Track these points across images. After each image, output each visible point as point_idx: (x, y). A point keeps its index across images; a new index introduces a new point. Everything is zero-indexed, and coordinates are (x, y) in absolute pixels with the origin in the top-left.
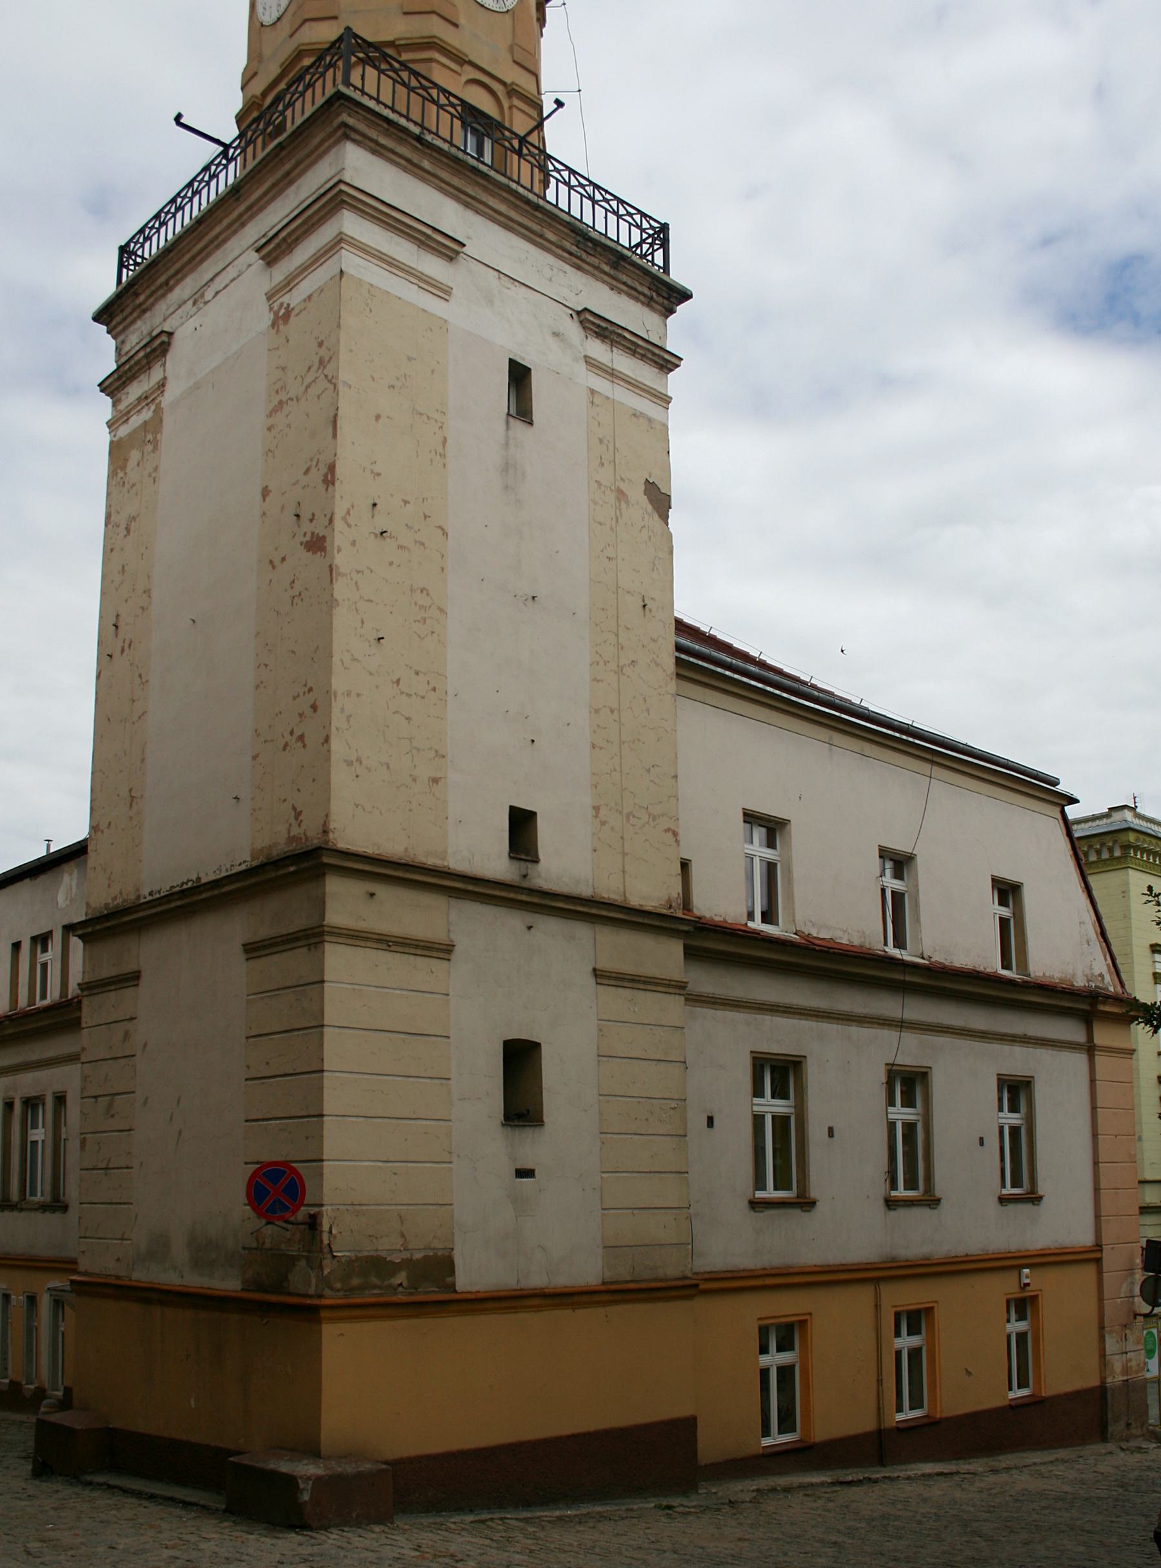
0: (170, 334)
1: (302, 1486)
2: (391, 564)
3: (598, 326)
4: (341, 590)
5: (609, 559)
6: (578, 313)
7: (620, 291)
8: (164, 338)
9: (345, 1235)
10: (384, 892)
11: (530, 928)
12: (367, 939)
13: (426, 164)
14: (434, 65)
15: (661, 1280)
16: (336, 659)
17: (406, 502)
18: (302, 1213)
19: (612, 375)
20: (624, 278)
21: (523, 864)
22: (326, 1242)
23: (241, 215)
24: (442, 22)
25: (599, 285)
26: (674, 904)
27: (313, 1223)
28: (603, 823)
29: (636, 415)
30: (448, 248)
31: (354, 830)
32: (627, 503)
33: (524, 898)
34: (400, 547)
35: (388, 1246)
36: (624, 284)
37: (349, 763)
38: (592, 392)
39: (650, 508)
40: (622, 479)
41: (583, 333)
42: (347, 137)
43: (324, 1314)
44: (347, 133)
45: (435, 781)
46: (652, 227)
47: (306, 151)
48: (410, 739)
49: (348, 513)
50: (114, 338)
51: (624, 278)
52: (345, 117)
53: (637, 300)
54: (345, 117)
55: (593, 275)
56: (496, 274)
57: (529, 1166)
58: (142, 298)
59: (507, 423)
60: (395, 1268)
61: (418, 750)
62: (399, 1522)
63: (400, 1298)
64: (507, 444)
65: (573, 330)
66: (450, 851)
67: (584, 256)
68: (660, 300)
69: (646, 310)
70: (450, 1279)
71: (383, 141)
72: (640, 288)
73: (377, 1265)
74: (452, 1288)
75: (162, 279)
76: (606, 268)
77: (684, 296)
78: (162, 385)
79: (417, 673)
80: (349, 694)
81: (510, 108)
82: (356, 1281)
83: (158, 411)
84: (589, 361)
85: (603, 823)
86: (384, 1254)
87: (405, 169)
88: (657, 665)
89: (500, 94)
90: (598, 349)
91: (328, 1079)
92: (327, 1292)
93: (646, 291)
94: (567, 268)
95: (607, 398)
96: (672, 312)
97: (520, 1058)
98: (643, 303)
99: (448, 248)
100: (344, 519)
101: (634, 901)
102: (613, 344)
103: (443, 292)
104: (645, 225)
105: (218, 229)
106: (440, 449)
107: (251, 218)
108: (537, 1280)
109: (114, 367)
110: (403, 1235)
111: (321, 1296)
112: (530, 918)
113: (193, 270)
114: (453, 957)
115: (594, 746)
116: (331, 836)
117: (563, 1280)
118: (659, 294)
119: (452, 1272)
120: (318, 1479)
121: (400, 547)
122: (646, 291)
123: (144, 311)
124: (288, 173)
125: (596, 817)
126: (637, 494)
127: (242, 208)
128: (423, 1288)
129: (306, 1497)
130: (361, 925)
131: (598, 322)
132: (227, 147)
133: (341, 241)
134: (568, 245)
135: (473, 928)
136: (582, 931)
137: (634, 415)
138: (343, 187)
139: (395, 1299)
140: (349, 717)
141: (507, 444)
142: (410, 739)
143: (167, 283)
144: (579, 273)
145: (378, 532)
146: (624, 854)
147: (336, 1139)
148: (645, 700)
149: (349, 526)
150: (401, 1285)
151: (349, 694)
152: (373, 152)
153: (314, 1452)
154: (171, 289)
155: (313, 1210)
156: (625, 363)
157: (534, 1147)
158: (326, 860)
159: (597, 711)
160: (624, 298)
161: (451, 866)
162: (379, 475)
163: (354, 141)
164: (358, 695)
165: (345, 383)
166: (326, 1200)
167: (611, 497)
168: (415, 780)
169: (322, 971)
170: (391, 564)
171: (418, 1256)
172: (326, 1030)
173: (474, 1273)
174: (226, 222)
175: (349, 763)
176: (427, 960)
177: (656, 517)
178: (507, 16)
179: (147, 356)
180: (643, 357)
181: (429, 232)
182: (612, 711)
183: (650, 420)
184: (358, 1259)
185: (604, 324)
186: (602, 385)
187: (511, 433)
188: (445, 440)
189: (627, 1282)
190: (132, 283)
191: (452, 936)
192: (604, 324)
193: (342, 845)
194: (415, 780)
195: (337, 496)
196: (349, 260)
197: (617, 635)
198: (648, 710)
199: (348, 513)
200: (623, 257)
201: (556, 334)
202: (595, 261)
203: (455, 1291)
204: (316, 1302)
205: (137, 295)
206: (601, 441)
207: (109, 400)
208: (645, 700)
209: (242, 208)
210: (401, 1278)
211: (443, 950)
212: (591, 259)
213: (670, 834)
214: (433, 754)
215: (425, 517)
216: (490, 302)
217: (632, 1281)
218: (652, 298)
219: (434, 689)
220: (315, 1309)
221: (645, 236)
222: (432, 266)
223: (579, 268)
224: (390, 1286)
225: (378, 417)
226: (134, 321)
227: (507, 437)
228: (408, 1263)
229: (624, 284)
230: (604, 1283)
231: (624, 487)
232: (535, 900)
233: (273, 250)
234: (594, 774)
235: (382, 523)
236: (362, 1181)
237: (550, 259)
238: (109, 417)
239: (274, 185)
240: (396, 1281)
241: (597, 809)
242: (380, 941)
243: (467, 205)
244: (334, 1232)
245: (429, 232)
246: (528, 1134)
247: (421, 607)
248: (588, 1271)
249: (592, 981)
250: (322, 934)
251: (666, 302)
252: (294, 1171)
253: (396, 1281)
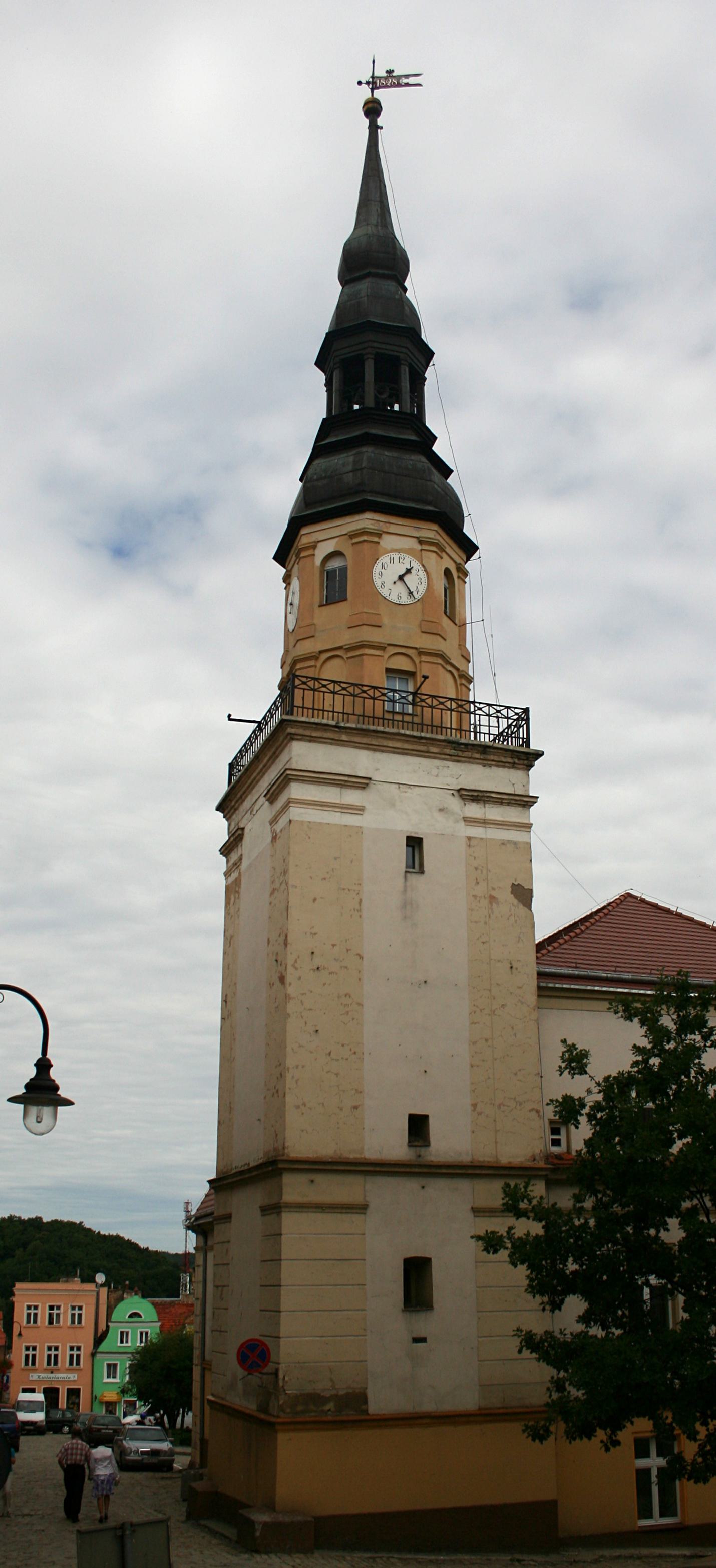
0: (243, 829)
1: (257, 1527)
2: (325, 984)
3: (472, 796)
4: (291, 1008)
5: (484, 943)
6: (459, 790)
7: (490, 766)
8: (240, 832)
9: (293, 1382)
10: (319, 1178)
11: (423, 1187)
12: (308, 1207)
13: (344, 738)
14: (364, 657)
15: (527, 1407)
16: (289, 1049)
17: (334, 945)
18: (270, 1368)
19: (484, 823)
20: (492, 757)
21: (418, 1149)
22: (281, 1384)
23: (262, 770)
24: (370, 628)
25: (475, 767)
26: (537, 1158)
27: (276, 1373)
28: (480, 1114)
29: (503, 843)
30: (362, 783)
31: (302, 1141)
32: (498, 903)
33: (416, 1170)
34: (331, 973)
35: (322, 1386)
36: (493, 761)
37: (298, 1107)
38: (469, 838)
39: (515, 901)
40: (494, 889)
41: (462, 802)
42: (293, 739)
43: (278, 1427)
44: (292, 737)
45: (356, 1107)
46: (516, 714)
47: (279, 744)
48: (338, 1086)
49: (296, 961)
50: (227, 820)
51: (492, 757)
52: (290, 730)
53: (504, 767)
54: (290, 730)
55: (469, 762)
56: (397, 786)
57: (422, 1335)
58: (233, 803)
59: (405, 877)
60: (326, 1400)
61: (344, 1091)
62: (317, 1554)
63: (330, 1418)
64: (405, 891)
65: (455, 804)
66: (366, 1147)
67: (460, 754)
68: (521, 762)
69: (512, 771)
70: (363, 1407)
71: (314, 735)
72: (504, 760)
73: (315, 1399)
74: (366, 1412)
75: (239, 795)
76: (477, 756)
77: (539, 755)
78: (241, 859)
79: (343, 1045)
80: (297, 1067)
81: (420, 662)
82: (300, 1408)
83: (240, 873)
84: (468, 820)
85: (480, 1114)
86: (318, 1392)
87: (331, 744)
88: (522, 1003)
89: (413, 656)
90: (474, 810)
91: (283, 1291)
92: (282, 1414)
93: (510, 760)
94: (450, 764)
95: (482, 839)
96: (532, 766)
97: (416, 1272)
98: (509, 768)
99: (362, 783)
100: (293, 966)
101: (504, 1160)
102: (485, 802)
103: (359, 810)
104: (511, 714)
105: (255, 775)
106: (357, 907)
107: (266, 771)
108: (428, 1407)
109: (227, 838)
110: (332, 1380)
111: (278, 1417)
112: (423, 1181)
113: (250, 792)
114: (368, 1212)
115: (472, 1066)
116: (286, 1151)
117: (447, 1407)
118: (519, 759)
119: (365, 1401)
120: (265, 1524)
121: (331, 973)
122: (510, 760)
123: (236, 810)
124: (275, 753)
125: (474, 1110)
126: (505, 896)
127: (261, 766)
128: (345, 1411)
129: (258, 1534)
130: (305, 1200)
131: (470, 793)
132: (259, 723)
133: (290, 802)
134: (447, 751)
135: (380, 1192)
136: (464, 1185)
137: (503, 844)
138: (288, 772)
139: (325, 1419)
140: (297, 1081)
141: (405, 891)
142: (338, 1086)
143: (241, 797)
144: (459, 764)
145: (315, 967)
146: (496, 1131)
147: (287, 1325)
148: (513, 1028)
149: (296, 969)
150: (329, 1410)
151: (297, 1067)
152: (310, 741)
153: (270, 1506)
154: (244, 801)
155: (277, 1366)
156: (494, 812)
157: (423, 1324)
158: (280, 1166)
159: (474, 1043)
160: (494, 769)
161: (367, 1156)
162: (315, 934)
163: (298, 740)
164: (303, 1066)
165: (293, 886)
166: (281, 1360)
167: (485, 902)
168: (341, 1109)
169: (280, 1228)
170: (325, 984)
171: (342, 1392)
172: (283, 1262)
173: (380, 1402)
174: (257, 771)
175: (298, 1107)
176: (350, 1215)
177: (521, 906)
178: (418, 603)
179: (235, 840)
180: (509, 804)
181: (346, 779)
182: (486, 1040)
183: (515, 843)
184: (301, 1395)
185: (475, 794)
186: (477, 832)
187: (408, 883)
188: (361, 900)
189: (499, 1408)
190: (238, 782)
191: (367, 1199)
192: (475, 794)
193: (293, 1155)
194: (341, 1109)
195: (289, 953)
196: (295, 812)
197: (490, 991)
198: (515, 1035)
199: (296, 961)
200: (489, 747)
201: (441, 810)
202: (469, 754)
203: (368, 1414)
204: (273, 1420)
205: (231, 801)
206: (476, 868)
207: (224, 859)
208: (513, 1028)
209: (261, 766)
210: (330, 1406)
211: (362, 1208)
212: (466, 754)
213: (534, 1113)
214: (354, 1092)
215: (348, 951)
216: (392, 805)
217: (503, 1408)
218: (514, 763)
219: (355, 1053)
220: (271, 1425)
221: (510, 721)
222: (352, 797)
223: (458, 761)
224: (323, 1411)
225: (315, 900)
226: (232, 814)
227: (405, 886)
228: (336, 1398)
229: (493, 761)
230: (480, 1409)
231: (494, 893)
232: (425, 1170)
233: (272, 796)
234: (472, 1083)
235: (318, 961)
236: (305, 1347)
237: (437, 763)
238: (225, 869)
239: (271, 758)
240: (327, 1408)
241: (474, 1106)
242: (316, 1208)
243: (375, 750)
244: (286, 1378)
245: (346, 779)
246: (422, 1316)
247: (345, 1005)
248: (469, 1401)
249: (471, 1215)
250: (280, 1207)
251: (526, 762)
252: (263, 1344)
253: (327, 1408)
